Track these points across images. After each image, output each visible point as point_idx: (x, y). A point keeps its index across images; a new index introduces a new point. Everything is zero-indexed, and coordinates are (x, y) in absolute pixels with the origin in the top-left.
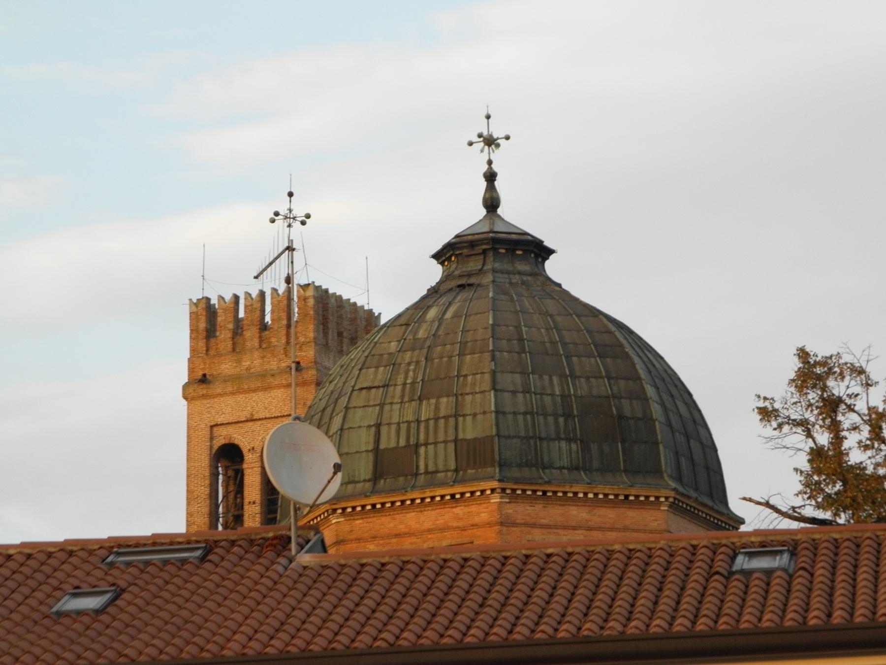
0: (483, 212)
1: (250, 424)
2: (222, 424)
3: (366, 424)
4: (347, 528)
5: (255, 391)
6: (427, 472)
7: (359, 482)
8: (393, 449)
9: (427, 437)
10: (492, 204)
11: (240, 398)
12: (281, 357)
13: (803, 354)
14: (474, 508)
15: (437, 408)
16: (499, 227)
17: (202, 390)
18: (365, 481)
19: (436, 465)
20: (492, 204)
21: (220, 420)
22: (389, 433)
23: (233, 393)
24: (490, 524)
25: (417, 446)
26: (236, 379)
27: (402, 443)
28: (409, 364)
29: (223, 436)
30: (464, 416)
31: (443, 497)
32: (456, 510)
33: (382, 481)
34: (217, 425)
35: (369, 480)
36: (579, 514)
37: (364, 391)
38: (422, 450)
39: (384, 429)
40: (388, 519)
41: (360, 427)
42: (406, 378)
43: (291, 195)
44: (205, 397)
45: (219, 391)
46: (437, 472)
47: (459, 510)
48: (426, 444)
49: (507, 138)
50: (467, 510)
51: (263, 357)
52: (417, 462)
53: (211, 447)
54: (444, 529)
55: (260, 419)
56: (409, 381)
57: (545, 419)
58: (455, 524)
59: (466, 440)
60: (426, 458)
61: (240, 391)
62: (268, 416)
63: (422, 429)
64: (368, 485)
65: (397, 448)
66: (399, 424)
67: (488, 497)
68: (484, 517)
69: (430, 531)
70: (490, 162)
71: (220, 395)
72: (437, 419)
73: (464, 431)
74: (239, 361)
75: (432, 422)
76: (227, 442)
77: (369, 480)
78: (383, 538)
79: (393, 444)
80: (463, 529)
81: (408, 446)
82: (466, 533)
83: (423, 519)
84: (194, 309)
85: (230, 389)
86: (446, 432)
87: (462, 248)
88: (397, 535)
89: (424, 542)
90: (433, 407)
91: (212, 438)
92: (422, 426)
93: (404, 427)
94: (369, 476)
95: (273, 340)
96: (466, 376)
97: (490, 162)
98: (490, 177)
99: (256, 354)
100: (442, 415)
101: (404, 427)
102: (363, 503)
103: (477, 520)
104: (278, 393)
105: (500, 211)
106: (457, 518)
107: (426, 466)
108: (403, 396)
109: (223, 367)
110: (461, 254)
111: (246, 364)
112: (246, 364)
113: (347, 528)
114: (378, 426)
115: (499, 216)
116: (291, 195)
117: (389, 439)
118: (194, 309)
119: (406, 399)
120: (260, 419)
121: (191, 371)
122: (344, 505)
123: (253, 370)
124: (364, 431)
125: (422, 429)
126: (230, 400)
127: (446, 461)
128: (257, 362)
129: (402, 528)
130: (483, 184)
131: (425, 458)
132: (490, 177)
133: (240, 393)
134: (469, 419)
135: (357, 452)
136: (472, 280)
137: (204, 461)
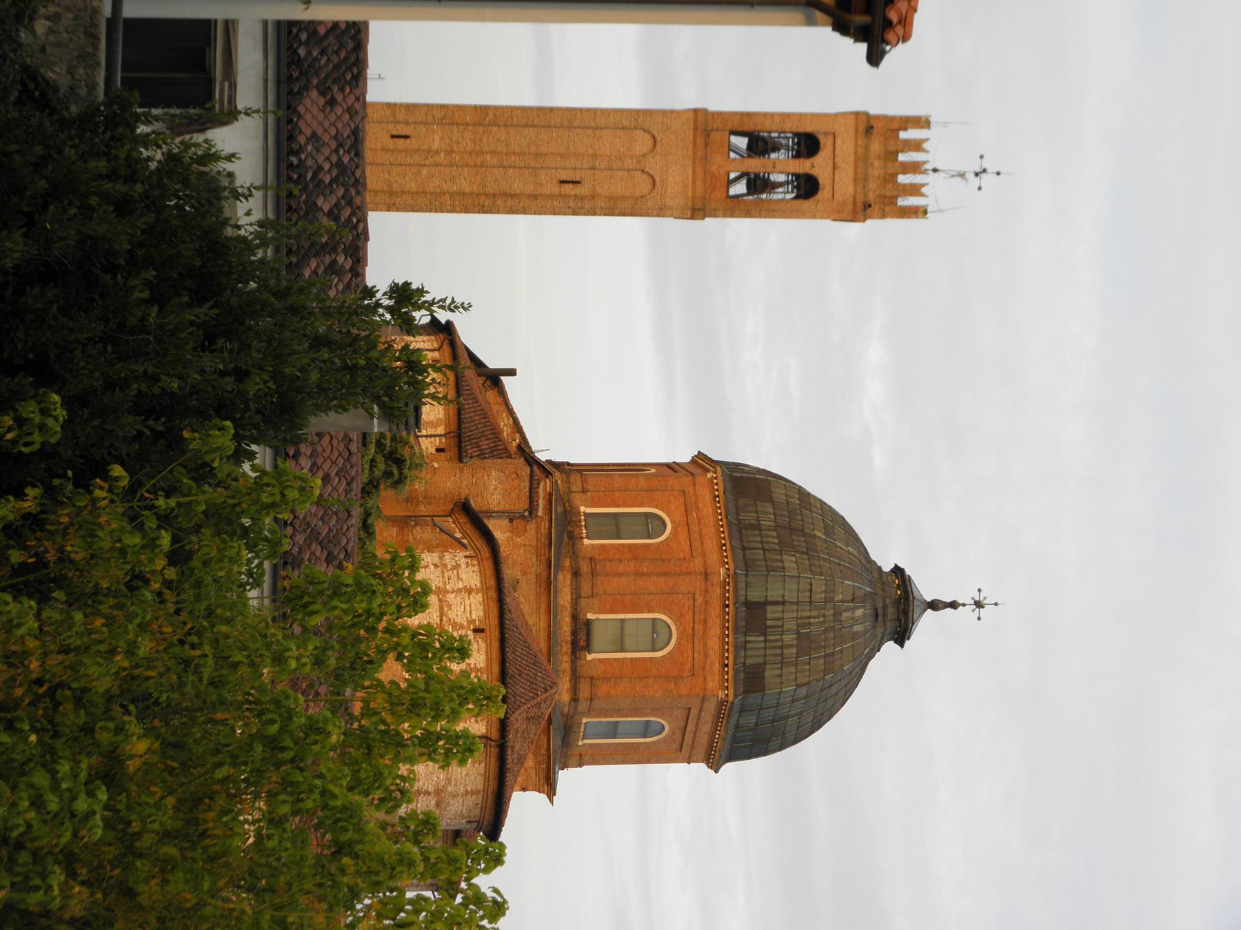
0: (929, 600)
1: (832, 164)
2: (834, 143)
3: (786, 594)
4: (716, 582)
5: (855, 170)
6: (746, 642)
7: (746, 591)
8: (765, 616)
9: (770, 641)
10: (935, 605)
11: (852, 158)
12: (877, 193)
13: (874, 58)
14: (717, 677)
15: (790, 646)
16: (917, 611)
17: (862, 128)
18: (746, 595)
19: (750, 649)
20: (935, 605)
21: (838, 141)
22: (777, 612)
23: (856, 153)
24: (705, 689)
25: (765, 634)
26: (866, 157)
27: (769, 623)
28: (824, 616)
29: (826, 143)
30: (781, 668)
31: (727, 658)
32: (717, 664)
33: (744, 609)
34: (835, 138)
35: (746, 599)
36: (706, 728)
37: (809, 587)
38: (762, 638)
39: (780, 608)
40: (717, 613)
41: (784, 589)
42: (815, 617)
43: (998, 173)
44: (857, 129)
45: (859, 142)
46: (745, 650)
47: (717, 667)
48: (765, 641)
49: (979, 619)
50: (716, 672)
51: (878, 177)
52: (754, 636)
53: (819, 133)
54: (706, 655)
55: (834, 174)
56: (812, 620)
57: (779, 668)
58: (708, 663)
59: (764, 670)
60: (757, 642)
61: (856, 158)
62: (836, 181)
63: (776, 637)
64: (743, 599)
65: (766, 619)
66: (783, 619)
67: (723, 690)
68: (710, 685)
69: (705, 644)
70: (964, 605)
71: (856, 142)
72: (781, 647)
73: (771, 669)
74: (879, 157)
75: (780, 644)
76: (822, 145)
77: (746, 599)
78: (705, 610)
79: (769, 615)
80: (703, 669)
81: (766, 627)
82: (701, 672)
83: (714, 639)
84: (923, 120)
85: (860, 151)
86: (772, 655)
87: (904, 604)
88: (705, 621)
89: (699, 640)
90: (791, 643)
91: (826, 134)
92: (779, 637)
93: (780, 623)
94: (749, 598)
95: (890, 186)
96: (809, 663)
97: (964, 605)
98: (953, 605)
99: (882, 172)
100: (784, 651)
101: (780, 623)
102: (730, 599)
103: (709, 679)
104: (851, 189)
105: (929, 611)
106: (712, 664)
107: (750, 642)
108: (802, 618)
109: (877, 144)
110: (900, 603)
111: (876, 163)
112: (876, 163)
113: (716, 582)
114: (783, 603)
115: (924, 611)
116: (998, 173)
117: (773, 612)
118: (923, 120)
119: (799, 621)
120: (834, 174)
121: (878, 118)
122: (731, 584)
123: (870, 169)
124: (780, 592)
125: (776, 637)
126: (851, 150)
127: (752, 656)
128: (876, 173)
129: (710, 623)
130: (948, 600)
131: (756, 639)
132: (953, 605)
133: (855, 159)
134: (779, 672)
135: (767, 589)
136: (880, 618)
137: (808, 128)
